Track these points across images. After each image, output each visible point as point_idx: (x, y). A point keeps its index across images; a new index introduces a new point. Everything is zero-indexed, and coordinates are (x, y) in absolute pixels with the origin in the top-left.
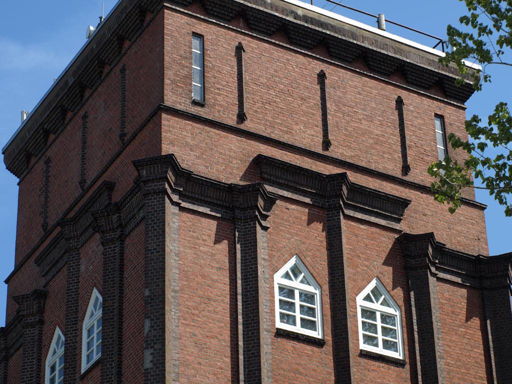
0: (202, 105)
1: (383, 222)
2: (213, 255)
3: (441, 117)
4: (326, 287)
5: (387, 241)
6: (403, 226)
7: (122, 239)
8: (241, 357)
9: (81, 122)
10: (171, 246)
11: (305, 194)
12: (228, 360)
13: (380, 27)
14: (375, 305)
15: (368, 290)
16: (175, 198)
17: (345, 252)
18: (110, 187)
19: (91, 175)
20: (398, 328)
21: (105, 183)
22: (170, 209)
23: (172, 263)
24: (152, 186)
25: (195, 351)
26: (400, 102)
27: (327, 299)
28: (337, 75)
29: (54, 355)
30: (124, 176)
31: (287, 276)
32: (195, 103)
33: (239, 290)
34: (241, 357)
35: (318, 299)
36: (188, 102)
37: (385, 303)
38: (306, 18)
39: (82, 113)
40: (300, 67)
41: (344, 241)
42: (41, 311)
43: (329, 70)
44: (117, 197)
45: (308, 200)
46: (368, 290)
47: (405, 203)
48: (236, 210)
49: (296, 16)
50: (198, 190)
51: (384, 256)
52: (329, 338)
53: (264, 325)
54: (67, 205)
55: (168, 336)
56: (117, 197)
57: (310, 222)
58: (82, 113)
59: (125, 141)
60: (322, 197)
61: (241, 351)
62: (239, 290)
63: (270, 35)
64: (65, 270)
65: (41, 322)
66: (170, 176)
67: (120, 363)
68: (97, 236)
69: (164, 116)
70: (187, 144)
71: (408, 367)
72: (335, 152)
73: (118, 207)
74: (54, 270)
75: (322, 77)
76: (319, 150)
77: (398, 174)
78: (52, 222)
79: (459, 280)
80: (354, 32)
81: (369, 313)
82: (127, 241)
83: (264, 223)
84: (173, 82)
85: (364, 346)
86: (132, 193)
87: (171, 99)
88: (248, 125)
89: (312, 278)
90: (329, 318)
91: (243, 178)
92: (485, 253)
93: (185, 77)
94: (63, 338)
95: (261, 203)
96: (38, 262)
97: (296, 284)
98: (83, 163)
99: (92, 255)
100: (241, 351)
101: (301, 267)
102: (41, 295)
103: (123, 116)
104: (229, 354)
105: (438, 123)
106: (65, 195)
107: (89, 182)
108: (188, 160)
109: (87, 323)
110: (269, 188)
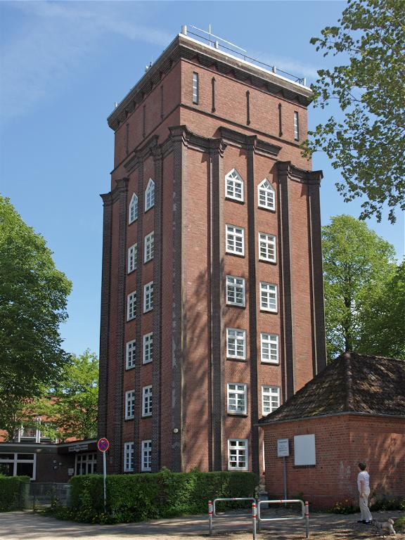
0: (197, 104)
1: (270, 156)
2: (201, 167)
3: (297, 112)
4: (246, 181)
5: (272, 163)
6: (278, 158)
7: (162, 159)
8: (211, 208)
9: (143, 109)
10: (185, 163)
11: (239, 143)
12: (206, 209)
13: (215, 47)
14: (265, 190)
15: (230, 173)
16: (186, 143)
17: (254, 167)
18: (157, 137)
19: (148, 132)
20: (274, 198)
21: (155, 135)
22: (184, 148)
23: (184, 169)
24: (176, 138)
25: (193, 205)
26: (280, 105)
27: (246, 186)
28: (256, 94)
29: (133, 204)
30: (163, 134)
31: (230, 176)
32: (194, 103)
33: (211, 181)
34: (211, 208)
35: (242, 186)
36: (191, 103)
37: (269, 188)
38: (242, 67)
39: (143, 105)
40: (271, 101)
41: (254, 163)
42: (127, 186)
43: (251, 90)
44: (160, 142)
45: (240, 146)
46: (230, 173)
47: (280, 148)
48: (211, 148)
49: (238, 66)
50: (195, 140)
51: (270, 170)
52: (246, 201)
53: (221, 196)
54: (138, 144)
55: (183, 198)
56: (160, 142)
57: (240, 155)
58: (143, 105)
59: (163, 118)
60: (246, 145)
61: (211, 205)
62: (211, 181)
63: (190, 60)
64: (137, 170)
65: (127, 190)
66: (184, 134)
67: (162, 208)
68: (151, 157)
69: (181, 108)
70: (191, 121)
71: (277, 213)
72: (252, 126)
73: (161, 146)
74: (133, 170)
75: (248, 93)
76: (274, 133)
77: (277, 136)
78: (131, 150)
79: (299, 180)
80: (263, 74)
81: (262, 192)
82: (165, 160)
83: (222, 155)
84: (185, 93)
85: (260, 205)
86: (167, 140)
87: (184, 101)
88: (216, 114)
89: (241, 177)
90: (246, 194)
91: (214, 136)
92: (310, 170)
93: (190, 92)
94: (137, 197)
95: (221, 146)
96: (125, 166)
97: (234, 180)
98: (144, 126)
99: (149, 164)
100: (211, 205)
101: (236, 173)
102: (127, 180)
103: (162, 108)
104: (206, 206)
105: (295, 115)
106: (136, 140)
107: (147, 135)
108: (191, 128)
109: (147, 192)
110: (225, 141)
